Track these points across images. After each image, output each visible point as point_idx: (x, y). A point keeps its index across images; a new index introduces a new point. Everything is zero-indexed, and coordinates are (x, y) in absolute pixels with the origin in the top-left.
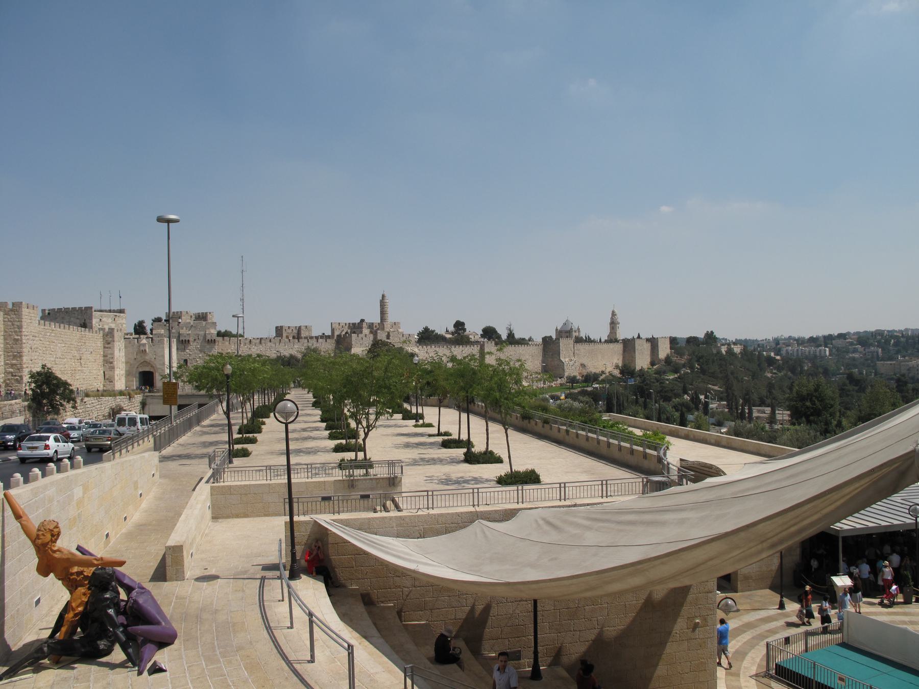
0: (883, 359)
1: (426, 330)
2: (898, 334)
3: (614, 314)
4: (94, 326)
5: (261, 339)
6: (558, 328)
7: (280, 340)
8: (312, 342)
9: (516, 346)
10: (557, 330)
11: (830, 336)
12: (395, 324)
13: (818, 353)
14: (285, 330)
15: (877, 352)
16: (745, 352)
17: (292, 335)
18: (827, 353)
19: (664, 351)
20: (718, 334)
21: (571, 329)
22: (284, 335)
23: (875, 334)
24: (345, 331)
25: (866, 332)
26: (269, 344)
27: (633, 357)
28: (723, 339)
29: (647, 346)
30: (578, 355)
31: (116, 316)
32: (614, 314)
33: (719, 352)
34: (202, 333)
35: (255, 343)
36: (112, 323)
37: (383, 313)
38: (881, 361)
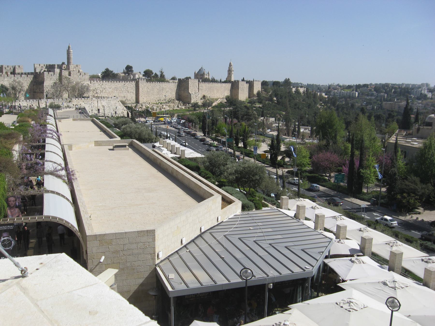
1: (107, 70)
2: (397, 87)
3: (230, 65)
8: (17, 77)
9: (161, 82)
10: (195, 73)
11: (359, 85)
12: (77, 66)
13: (351, 95)
14: (5, 68)
15: (384, 96)
16: (307, 93)
18: (357, 95)
19: (257, 88)
20: (292, 81)
22: (4, 71)
24: (44, 70)
25: (380, 84)
27: (237, 92)
28: (300, 83)
29: (246, 86)
30: (202, 90)
32: (230, 65)
33: (290, 92)
37: (69, 58)
38: (385, 101)
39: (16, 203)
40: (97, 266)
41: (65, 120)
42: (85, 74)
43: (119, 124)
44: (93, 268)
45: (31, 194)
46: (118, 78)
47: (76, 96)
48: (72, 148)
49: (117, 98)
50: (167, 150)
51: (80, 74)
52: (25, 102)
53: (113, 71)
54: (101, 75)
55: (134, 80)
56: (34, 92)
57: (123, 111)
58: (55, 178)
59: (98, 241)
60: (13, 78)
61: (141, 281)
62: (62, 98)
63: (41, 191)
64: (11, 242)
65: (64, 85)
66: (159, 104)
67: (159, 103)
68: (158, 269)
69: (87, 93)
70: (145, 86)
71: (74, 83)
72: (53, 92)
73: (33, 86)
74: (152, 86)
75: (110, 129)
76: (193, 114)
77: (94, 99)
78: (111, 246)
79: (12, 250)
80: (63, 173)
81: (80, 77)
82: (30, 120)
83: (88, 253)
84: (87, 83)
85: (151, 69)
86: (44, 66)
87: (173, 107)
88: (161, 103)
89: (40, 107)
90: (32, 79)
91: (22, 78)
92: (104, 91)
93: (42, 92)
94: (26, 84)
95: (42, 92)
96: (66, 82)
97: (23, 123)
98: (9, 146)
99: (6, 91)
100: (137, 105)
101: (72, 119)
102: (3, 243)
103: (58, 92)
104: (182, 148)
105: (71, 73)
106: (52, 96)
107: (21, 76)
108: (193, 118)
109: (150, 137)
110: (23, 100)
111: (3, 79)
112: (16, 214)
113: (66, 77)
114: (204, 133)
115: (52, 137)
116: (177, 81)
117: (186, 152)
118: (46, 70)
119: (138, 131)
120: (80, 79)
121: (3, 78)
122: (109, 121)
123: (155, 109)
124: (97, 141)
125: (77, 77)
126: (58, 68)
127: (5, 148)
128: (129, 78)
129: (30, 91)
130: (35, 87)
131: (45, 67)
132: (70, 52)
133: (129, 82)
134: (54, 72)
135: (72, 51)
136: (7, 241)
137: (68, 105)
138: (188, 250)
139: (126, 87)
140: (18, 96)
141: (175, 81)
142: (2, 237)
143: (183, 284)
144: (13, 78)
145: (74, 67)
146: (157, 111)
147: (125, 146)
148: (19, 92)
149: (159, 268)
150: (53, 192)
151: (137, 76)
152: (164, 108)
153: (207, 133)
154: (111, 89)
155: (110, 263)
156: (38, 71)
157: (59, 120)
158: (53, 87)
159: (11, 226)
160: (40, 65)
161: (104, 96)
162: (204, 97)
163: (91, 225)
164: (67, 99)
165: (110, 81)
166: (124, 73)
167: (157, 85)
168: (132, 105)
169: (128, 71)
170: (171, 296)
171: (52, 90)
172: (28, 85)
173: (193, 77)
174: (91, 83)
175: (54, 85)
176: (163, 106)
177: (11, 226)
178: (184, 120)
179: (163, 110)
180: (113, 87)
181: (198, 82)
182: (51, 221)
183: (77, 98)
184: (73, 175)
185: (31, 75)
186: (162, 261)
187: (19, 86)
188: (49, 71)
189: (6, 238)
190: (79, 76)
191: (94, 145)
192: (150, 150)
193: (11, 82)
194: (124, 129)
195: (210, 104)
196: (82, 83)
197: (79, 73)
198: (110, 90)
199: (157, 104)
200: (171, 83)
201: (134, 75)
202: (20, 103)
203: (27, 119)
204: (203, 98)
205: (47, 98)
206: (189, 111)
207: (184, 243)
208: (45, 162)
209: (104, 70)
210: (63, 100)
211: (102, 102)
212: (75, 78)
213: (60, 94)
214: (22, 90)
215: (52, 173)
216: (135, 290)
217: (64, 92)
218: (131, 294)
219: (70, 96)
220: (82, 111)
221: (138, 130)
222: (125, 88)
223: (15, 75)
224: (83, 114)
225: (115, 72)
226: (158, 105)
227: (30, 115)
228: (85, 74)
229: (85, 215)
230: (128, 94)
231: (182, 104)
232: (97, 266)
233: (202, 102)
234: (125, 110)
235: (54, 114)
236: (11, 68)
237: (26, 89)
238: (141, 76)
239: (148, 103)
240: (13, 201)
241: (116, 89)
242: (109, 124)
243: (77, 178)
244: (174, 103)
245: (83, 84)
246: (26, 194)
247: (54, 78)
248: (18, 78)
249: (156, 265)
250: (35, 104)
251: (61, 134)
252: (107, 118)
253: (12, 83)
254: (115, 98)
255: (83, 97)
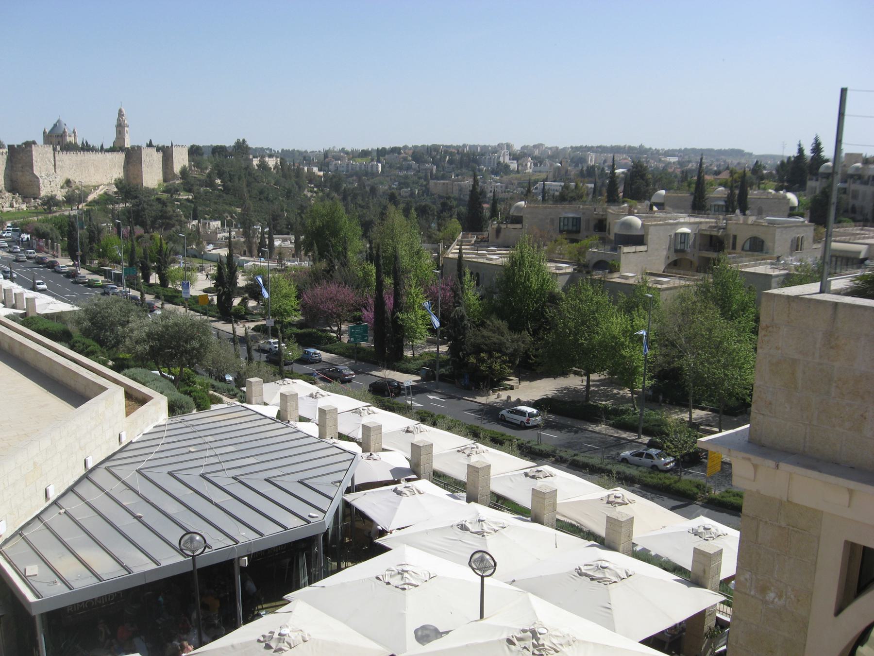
0: (437, 178)
2: (453, 150)
3: (121, 114)
6: (46, 130)
10: (44, 132)
11: (384, 149)
13: (369, 169)
16: (283, 167)
18: (380, 169)
19: (181, 160)
20: (252, 144)
21: (64, 132)
23: (431, 149)
25: (423, 146)
27: (139, 171)
28: (268, 149)
29: (158, 157)
30: (62, 167)
32: (121, 114)
33: (248, 167)
38: (434, 179)
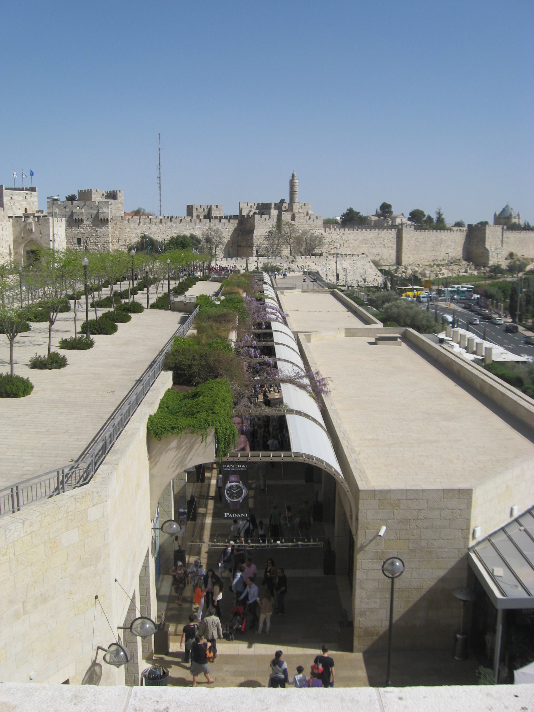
1: (351, 211)
4: (5, 203)
5: (172, 217)
7: (191, 220)
8: (214, 222)
10: (495, 215)
12: (305, 205)
14: (197, 209)
17: (203, 214)
22: (195, 214)
24: (253, 211)
26: (169, 223)
30: (507, 243)
31: (27, 194)
34: (95, 212)
35: (155, 223)
36: (23, 201)
39: (242, 427)
40: (371, 541)
41: (290, 291)
42: (317, 218)
43: (378, 300)
44: (365, 544)
45: (266, 414)
46: (368, 224)
47: (303, 253)
48: (310, 339)
49: (367, 256)
50: (460, 347)
51: (310, 218)
52: (225, 261)
53: (359, 213)
54: (341, 218)
55: (393, 226)
56: (238, 246)
57: (376, 277)
58: (297, 388)
59: (378, 501)
60: (208, 225)
61: (441, 573)
62: (281, 256)
63: (280, 411)
64: (242, 490)
65: (284, 236)
66: (435, 266)
67: (435, 264)
68: (473, 556)
69: (319, 248)
70: (412, 237)
71: (300, 231)
72: (267, 246)
73: (238, 236)
74: (423, 238)
75: (363, 308)
76: (493, 285)
77: (330, 257)
78: (397, 509)
79: (241, 503)
80: (306, 381)
81: (309, 223)
82: (241, 291)
83: (359, 518)
84: (319, 231)
85: (421, 209)
86: (255, 205)
87: (458, 271)
88: (438, 265)
89: (248, 269)
90: (236, 225)
91: (220, 225)
92: (346, 245)
93: (251, 246)
94: (226, 233)
95: (249, 247)
96: (288, 230)
97: (232, 296)
98: (223, 334)
99: (197, 243)
100: (398, 268)
101: (300, 290)
102: (229, 491)
103: (275, 246)
104: (487, 344)
105: (296, 216)
106: (264, 253)
107: (220, 222)
108: (493, 291)
109: (429, 323)
110: (221, 257)
111: (194, 225)
112: (241, 444)
113: (287, 223)
114: (513, 317)
115: (277, 319)
116: (465, 228)
117: (494, 351)
118: (257, 211)
119: (411, 313)
120: (309, 225)
121: (193, 224)
122: (357, 293)
123: (428, 275)
124: (350, 329)
125: (305, 222)
126: (275, 209)
127: (219, 337)
128: (385, 225)
129: (233, 244)
130: (240, 238)
131: (255, 207)
132: (295, 184)
133: (385, 230)
134: (269, 214)
135: (297, 181)
136: (235, 488)
137: (290, 267)
138: (522, 528)
139: (381, 239)
140: (214, 251)
141: (462, 229)
142: (228, 482)
143: (520, 588)
144: (208, 225)
145: (300, 206)
146: (432, 278)
147: (394, 339)
148: (217, 246)
149: (474, 554)
150: (299, 413)
151: (398, 221)
152: (443, 274)
153: (517, 317)
154: (357, 242)
155: (394, 539)
156: (244, 213)
157: (280, 292)
158: (267, 238)
159: (243, 466)
160: (248, 203)
161: (346, 253)
162: (511, 255)
163: (364, 472)
164: (288, 257)
165: (355, 228)
166: (377, 215)
167: (432, 235)
168: (390, 268)
169: (384, 212)
170: (500, 607)
171: (266, 243)
172: (230, 235)
173: (491, 221)
174: (325, 231)
175: (268, 236)
176: (441, 269)
177: (243, 466)
178: (478, 294)
179: (441, 276)
180: (361, 238)
181: (501, 231)
182: (295, 461)
183: (303, 256)
184: (325, 385)
185: (234, 220)
186: (479, 543)
187: (216, 236)
188: (262, 214)
189: (234, 484)
190: (308, 221)
191: (343, 335)
192: (437, 346)
193: (205, 230)
194: (387, 309)
195: (521, 268)
196: (312, 232)
197: (308, 216)
198: (356, 243)
199: (430, 266)
200: (455, 232)
201: (394, 219)
202: (218, 262)
203: (237, 289)
204: (509, 257)
205: (258, 255)
206: (485, 279)
207: (516, 514)
208: (278, 362)
209: (345, 211)
210: (282, 258)
211: (343, 262)
212: (301, 224)
213: (277, 249)
214: (221, 242)
215: (291, 381)
216: (430, 587)
217: (284, 246)
218: (423, 593)
219: (292, 252)
220: (315, 277)
221: (409, 311)
222: (379, 239)
223: (212, 220)
224: (316, 282)
225: (363, 214)
226: (433, 269)
227: (240, 282)
228: (317, 218)
229: (352, 454)
230: (384, 250)
231: (473, 268)
232: (371, 541)
233: (507, 264)
234: (379, 276)
235: (271, 280)
236: (205, 209)
237: (226, 242)
238: (405, 220)
239: (417, 265)
240: (238, 423)
241: (365, 241)
242: (360, 299)
243: (331, 390)
244: (460, 265)
245: (313, 234)
246: (258, 414)
247: (269, 224)
248: (215, 225)
249: (469, 549)
250: (240, 265)
251: (287, 315)
252: (350, 288)
253: (207, 232)
254: (363, 255)
255: (313, 255)
